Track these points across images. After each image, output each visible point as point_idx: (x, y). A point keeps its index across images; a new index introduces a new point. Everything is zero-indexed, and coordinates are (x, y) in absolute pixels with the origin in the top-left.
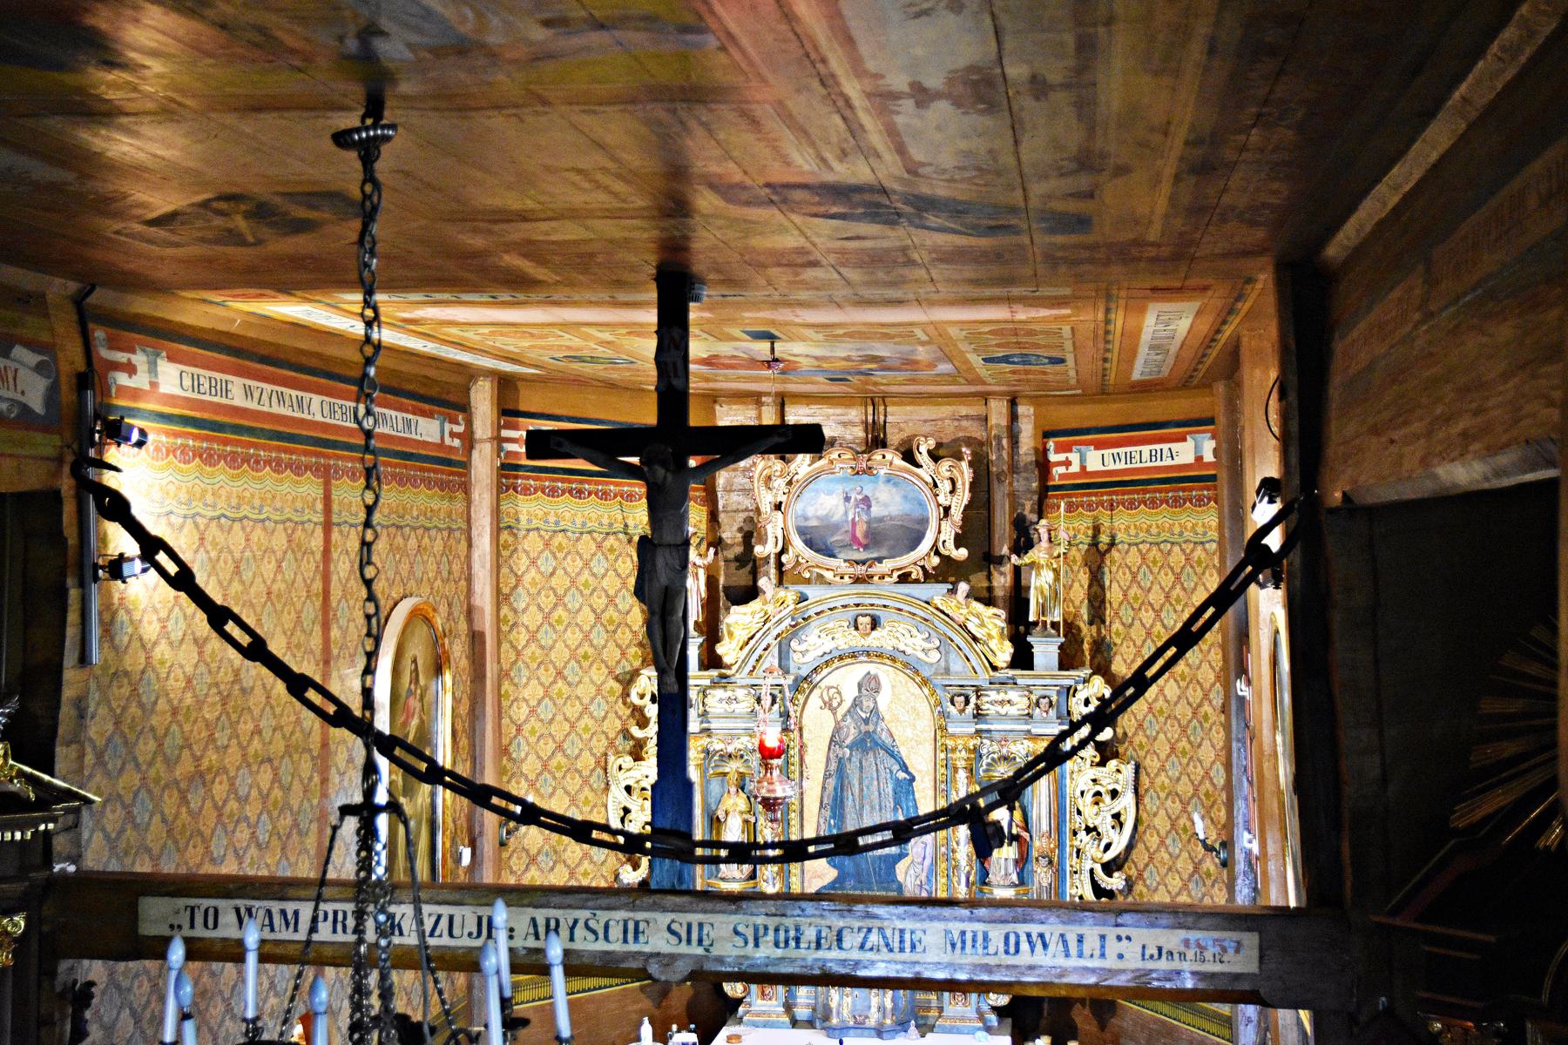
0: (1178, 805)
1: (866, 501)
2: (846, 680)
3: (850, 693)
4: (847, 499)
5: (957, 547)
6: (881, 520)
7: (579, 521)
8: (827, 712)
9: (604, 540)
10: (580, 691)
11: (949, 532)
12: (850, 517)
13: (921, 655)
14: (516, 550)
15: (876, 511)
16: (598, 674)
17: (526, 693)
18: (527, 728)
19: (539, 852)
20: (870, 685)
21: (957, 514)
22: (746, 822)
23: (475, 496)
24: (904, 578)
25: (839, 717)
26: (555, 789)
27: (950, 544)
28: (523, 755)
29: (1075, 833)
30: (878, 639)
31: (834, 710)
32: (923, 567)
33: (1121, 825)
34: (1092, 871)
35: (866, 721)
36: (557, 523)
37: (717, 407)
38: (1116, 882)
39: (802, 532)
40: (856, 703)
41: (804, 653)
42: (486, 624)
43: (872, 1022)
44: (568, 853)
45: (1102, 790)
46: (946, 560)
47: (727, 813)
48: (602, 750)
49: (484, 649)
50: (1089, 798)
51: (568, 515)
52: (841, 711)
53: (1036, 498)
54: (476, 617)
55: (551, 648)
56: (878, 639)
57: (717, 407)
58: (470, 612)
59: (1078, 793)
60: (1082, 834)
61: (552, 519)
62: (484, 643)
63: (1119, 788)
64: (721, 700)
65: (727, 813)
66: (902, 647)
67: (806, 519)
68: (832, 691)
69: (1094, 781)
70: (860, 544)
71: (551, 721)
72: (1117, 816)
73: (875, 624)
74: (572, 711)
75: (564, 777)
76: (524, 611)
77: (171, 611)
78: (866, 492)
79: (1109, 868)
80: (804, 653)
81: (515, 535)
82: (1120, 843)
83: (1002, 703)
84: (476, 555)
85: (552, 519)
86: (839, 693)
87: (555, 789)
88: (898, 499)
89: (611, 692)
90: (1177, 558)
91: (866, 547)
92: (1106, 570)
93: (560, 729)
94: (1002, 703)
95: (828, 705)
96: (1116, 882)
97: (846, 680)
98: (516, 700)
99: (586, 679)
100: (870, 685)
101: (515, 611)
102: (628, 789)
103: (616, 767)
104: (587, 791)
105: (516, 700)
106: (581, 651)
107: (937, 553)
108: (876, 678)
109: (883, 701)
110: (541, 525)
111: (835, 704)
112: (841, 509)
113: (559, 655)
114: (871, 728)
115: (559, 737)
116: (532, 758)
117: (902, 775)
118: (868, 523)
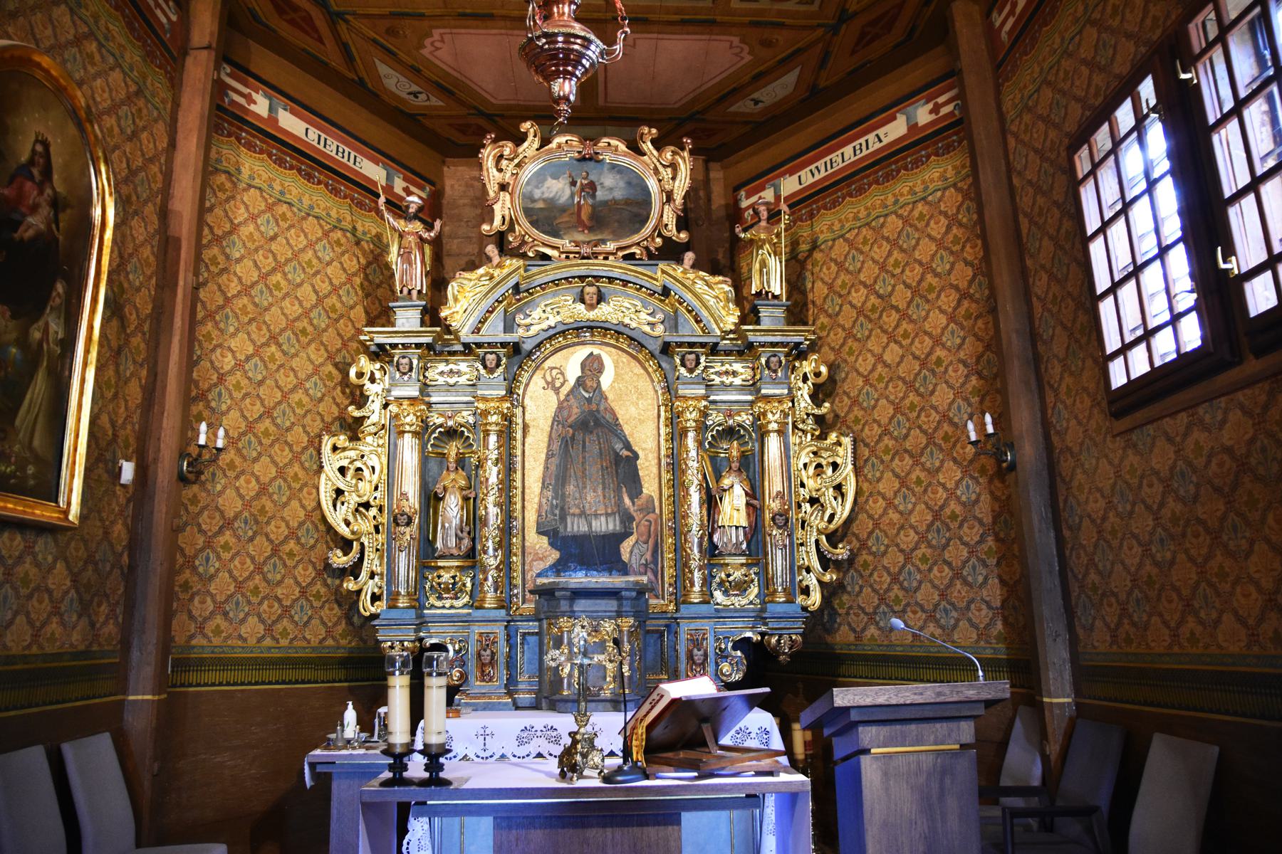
0: (908, 461)
1: (593, 186)
2: (571, 363)
3: (573, 372)
4: (573, 183)
5: (679, 231)
6: (605, 203)
7: (306, 202)
8: (551, 393)
9: (331, 231)
10: (295, 363)
11: (670, 218)
12: (576, 200)
13: (647, 329)
14: (233, 197)
15: (600, 195)
16: (319, 357)
17: (233, 344)
18: (231, 380)
19: (236, 517)
20: (592, 367)
21: (678, 198)
22: (466, 499)
23: (185, 100)
24: (630, 257)
25: (562, 397)
26: (260, 454)
27: (672, 226)
28: (224, 407)
29: (799, 506)
30: (604, 312)
31: (557, 391)
32: (647, 248)
33: (843, 495)
34: (817, 542)
35: (589, 400)
36: (282, 193)
37: (445, 169)
38: (842, 552)
39: (528, 212)
40: (580, 382)
41: (528, 326)
42: (184, 227)
43: (607, 694)
44: (272, 527)
45: (824, 463)
46: (667, 240)
47: (445, 489)
48: (317, 431)
49: (179, 255)
50: (811, 470)
51: (295, 192)
52: (565, 391)
53: (727, 245)
54: (173, 223)
55: (266, 309)
56: (604, 312)
57: (445, 169)
58: (164, 214)
59: (801, 466)
60: (806, 507)
61: (277, 187)
62: (179, 249)
63: (839, 461)
64: (442, 373)
65: (445, 489)
66: (627, 321)
67: (534, 201)
68: (554, 372)
69: (815, 453)
70: (585, 227)
71: (261, 383)
72: (838, 488)
73: (601, 298)
74: (287, 381)
75: (272, 445)
76: (238, 261)
77: (67, 592)
78: (592, 177)
79: (833, 538)
80: (528, 326)
81: (235, 185)
82: (843, 512)
83: (727, 373)
84: (179, 157)
85: (277, 187)
86: (562, 374)
87: (260, 454)
88: (622, 184)
89: (330, 375)
90: (894, 223)
91: (591, 229)
92: (808, 274)
93: (270, 394)
94: (727, 373)
95: (551, 385)
96: (842, 552)
97: (571, 363)
98: (220, 346)
99: (303, 354)
100: (592, 367)
101: (228, 257)
102: (342, 470)
103: (329, 446)
104: (297, 468)
105: (220, 346)
106: (299, 325)
107: (660, 235)
108: (599, 358)
109: (606, 380)
110: (265, 186)
111: (558, 385)
112: (568, 192)
113: (274, 318)
114: (594, 407)
115: (270, 403)
116: (234, 414)
117: (625, 453)
118: (593, 206)
